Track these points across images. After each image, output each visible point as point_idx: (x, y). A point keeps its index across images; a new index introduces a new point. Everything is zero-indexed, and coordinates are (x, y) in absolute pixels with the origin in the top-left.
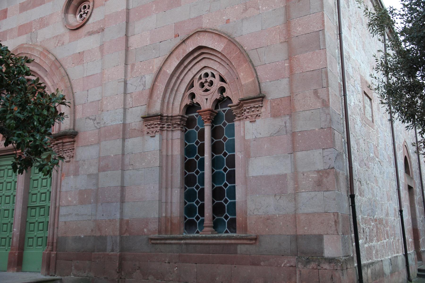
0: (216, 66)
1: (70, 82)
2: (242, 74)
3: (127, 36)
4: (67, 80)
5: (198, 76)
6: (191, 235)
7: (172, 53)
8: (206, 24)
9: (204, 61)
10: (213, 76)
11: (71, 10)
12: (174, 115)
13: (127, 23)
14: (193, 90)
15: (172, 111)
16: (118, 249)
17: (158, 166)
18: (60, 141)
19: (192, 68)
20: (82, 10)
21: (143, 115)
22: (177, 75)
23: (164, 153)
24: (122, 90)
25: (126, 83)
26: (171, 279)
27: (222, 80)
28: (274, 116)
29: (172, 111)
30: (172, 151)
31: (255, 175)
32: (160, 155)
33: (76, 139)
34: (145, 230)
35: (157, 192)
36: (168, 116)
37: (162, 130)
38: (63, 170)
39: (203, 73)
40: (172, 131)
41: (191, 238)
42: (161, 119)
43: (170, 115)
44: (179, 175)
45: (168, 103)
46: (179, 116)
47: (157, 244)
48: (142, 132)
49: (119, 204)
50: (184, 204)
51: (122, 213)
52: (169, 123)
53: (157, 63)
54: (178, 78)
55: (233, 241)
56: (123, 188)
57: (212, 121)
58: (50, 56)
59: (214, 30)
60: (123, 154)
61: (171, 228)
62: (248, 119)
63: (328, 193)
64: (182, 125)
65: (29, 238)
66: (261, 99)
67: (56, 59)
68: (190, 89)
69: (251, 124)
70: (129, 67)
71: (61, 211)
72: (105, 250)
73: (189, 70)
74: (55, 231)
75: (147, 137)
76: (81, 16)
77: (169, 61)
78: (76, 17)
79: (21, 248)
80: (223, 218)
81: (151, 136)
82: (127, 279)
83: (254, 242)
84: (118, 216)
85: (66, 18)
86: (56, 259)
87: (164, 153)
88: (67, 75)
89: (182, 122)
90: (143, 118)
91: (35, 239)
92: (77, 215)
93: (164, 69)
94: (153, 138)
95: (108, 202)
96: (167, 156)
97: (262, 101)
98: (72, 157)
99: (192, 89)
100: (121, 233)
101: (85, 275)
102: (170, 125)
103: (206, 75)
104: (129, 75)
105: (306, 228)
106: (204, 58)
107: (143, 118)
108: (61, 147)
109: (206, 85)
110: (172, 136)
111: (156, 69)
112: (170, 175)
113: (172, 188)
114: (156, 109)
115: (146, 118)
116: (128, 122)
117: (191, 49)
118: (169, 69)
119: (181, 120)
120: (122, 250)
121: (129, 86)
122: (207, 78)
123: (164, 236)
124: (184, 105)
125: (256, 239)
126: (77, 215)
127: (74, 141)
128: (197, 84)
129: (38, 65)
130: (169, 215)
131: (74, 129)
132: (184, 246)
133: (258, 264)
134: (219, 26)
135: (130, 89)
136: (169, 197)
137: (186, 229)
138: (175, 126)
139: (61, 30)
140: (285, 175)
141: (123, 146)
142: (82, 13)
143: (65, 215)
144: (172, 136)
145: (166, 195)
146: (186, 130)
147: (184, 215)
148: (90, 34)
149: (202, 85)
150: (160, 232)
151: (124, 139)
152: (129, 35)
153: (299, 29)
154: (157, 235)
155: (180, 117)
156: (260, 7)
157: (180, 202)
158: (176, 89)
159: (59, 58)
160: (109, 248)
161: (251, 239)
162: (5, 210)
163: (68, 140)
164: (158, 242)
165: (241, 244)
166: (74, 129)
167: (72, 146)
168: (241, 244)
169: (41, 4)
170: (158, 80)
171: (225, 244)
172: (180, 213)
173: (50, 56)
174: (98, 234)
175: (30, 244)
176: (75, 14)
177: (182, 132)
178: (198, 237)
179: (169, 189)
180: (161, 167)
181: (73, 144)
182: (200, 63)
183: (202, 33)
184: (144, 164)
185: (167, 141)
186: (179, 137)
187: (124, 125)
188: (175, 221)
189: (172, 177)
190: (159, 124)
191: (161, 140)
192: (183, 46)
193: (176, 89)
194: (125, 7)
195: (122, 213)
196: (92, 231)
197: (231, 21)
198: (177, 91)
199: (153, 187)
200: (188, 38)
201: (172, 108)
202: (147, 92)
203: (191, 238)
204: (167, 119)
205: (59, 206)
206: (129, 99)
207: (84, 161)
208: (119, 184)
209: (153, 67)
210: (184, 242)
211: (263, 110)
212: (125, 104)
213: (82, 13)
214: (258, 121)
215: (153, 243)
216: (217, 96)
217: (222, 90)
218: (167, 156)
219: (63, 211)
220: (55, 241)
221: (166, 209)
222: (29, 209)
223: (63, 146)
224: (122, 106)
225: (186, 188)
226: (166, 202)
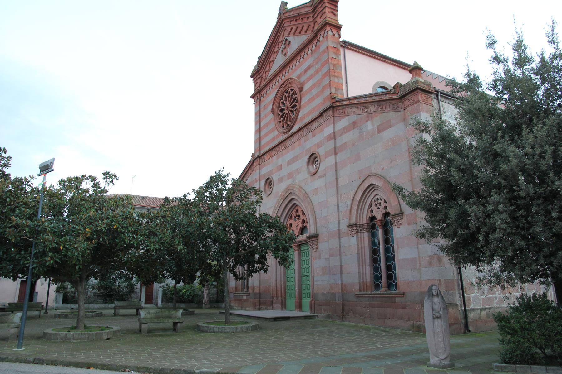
1: (313, 205)
2: (392, 200)
3: (336, 178)
4: (311, 205)
5: (374, 200)
6: (378, 292)
8: (373, 171)
10: (381, 200)
12: (363, 223)
13: (336, 171)
14: (372, 208)
16: (341, 300)
18: (311, 240)
19: (370, 195)
21: (347, 225)
22: (363, 200)
23: (360, 246)
24: (336, 210)
25: (338, 206)
26: (366, 316)
28: (409, 224)
31: (401, 258)
33: (318, 238)
34: (353, 289)
35: (357, 268)
36: (360, 225)
39: (376, 198)
40: (363, 232)
41: (374, 294)
43: (361, 224)
45: (360, 216)
48: (348, 234)
49: (340, 275)
50: (373, 274)
51: (342, 280)
54: (363, 202)
55: (393, 296)
56: (341, 266)
58: (303, 191)
59: (377, 174)
60: (340, 247)
61: (367, 288)
62: (396, 226)
63: (434, 268)
68: (370, 208)
69: (398, 229)
72: (335, 300)
75: (351, 237)
76: (316, 166)
79: (300, 299)
80: (392, 282)
82: (347, 316)
83: (403, 296)
86: (315, 305)
87: (360, 246)
88: (311, 201)
89: (368, 227)
90: (348, 226)
91: (306, 294)
93: (356, 197)
94: (353, 238)
95: (335, 274)
96: (362, 247)
97: (402, 215)
101: (328, 313)
103: (378, 199)
106: (375, 190)
107: (348, 226)
109: (378, 205)
110: (364, 235)
111: (352, 198)
112: (364, 258)
114: (354, 221)
115: (349, 226)
116: (341, 228)
117: (367, 186)
118: (358, 198)
120: (343, 301)
123: (362, 292)
124: (368, 217)
125: (404, 294)
126: (322, 281)
127: (317, 240)
128: (373, 204)
129: (296, 195)
132: (371, 298)
133: (405, 308)
134: (379, 172)
135: (341, 209)
137: (375, 288)
139: (307, 176)
140: (415, 258)
141: (340, 243)
142: (316, 164)
144: (364, 235)
146: (372, 231)
147: (373, 280)
148: (320, 177)
149: (376, 205)
150: (360, 291)
151: (340, 238)
154: (359, 292)
157: (370, 273)
159: (307, 191)
160: (337, 299)
161: (401, 294)
164: (359, 296)
166: (316, 233)
169: (296, 161)
171: (390, 297)
172: (371, 280)
173: (303, 191)
174: (332, 292)
175: (304, 296)
176: (313, 165)
179: (364, 266)
180: (358, 254)
183: (371, 176)
185: (361, 238)
186: (367, 236)
187: (339, 230)
188: (368, 284)
189: (365, 259)
190: (356, 229)
191: (357, 239)
193: (363, 208)
194: (334, 162)
195: (342, 280)
196: (329, 290)
197: (385, 169)
198: (364, 209)
200: (365, 179)
201: (362, 219)
203: (374, 294)
204: (360, 226)
206: (341, 216)
207: (323, 250)
211: (403, 220)
212: (339, 218)
213: (316, 164)
214: (401, 227)
215: (357, 297)
216: (384, 212)
217: (386, 208)
218: (362, 247)
219: (315, 279)
221: (363, 277)
223: (312, 242)
224: (337, 220)
226: (363, 274)
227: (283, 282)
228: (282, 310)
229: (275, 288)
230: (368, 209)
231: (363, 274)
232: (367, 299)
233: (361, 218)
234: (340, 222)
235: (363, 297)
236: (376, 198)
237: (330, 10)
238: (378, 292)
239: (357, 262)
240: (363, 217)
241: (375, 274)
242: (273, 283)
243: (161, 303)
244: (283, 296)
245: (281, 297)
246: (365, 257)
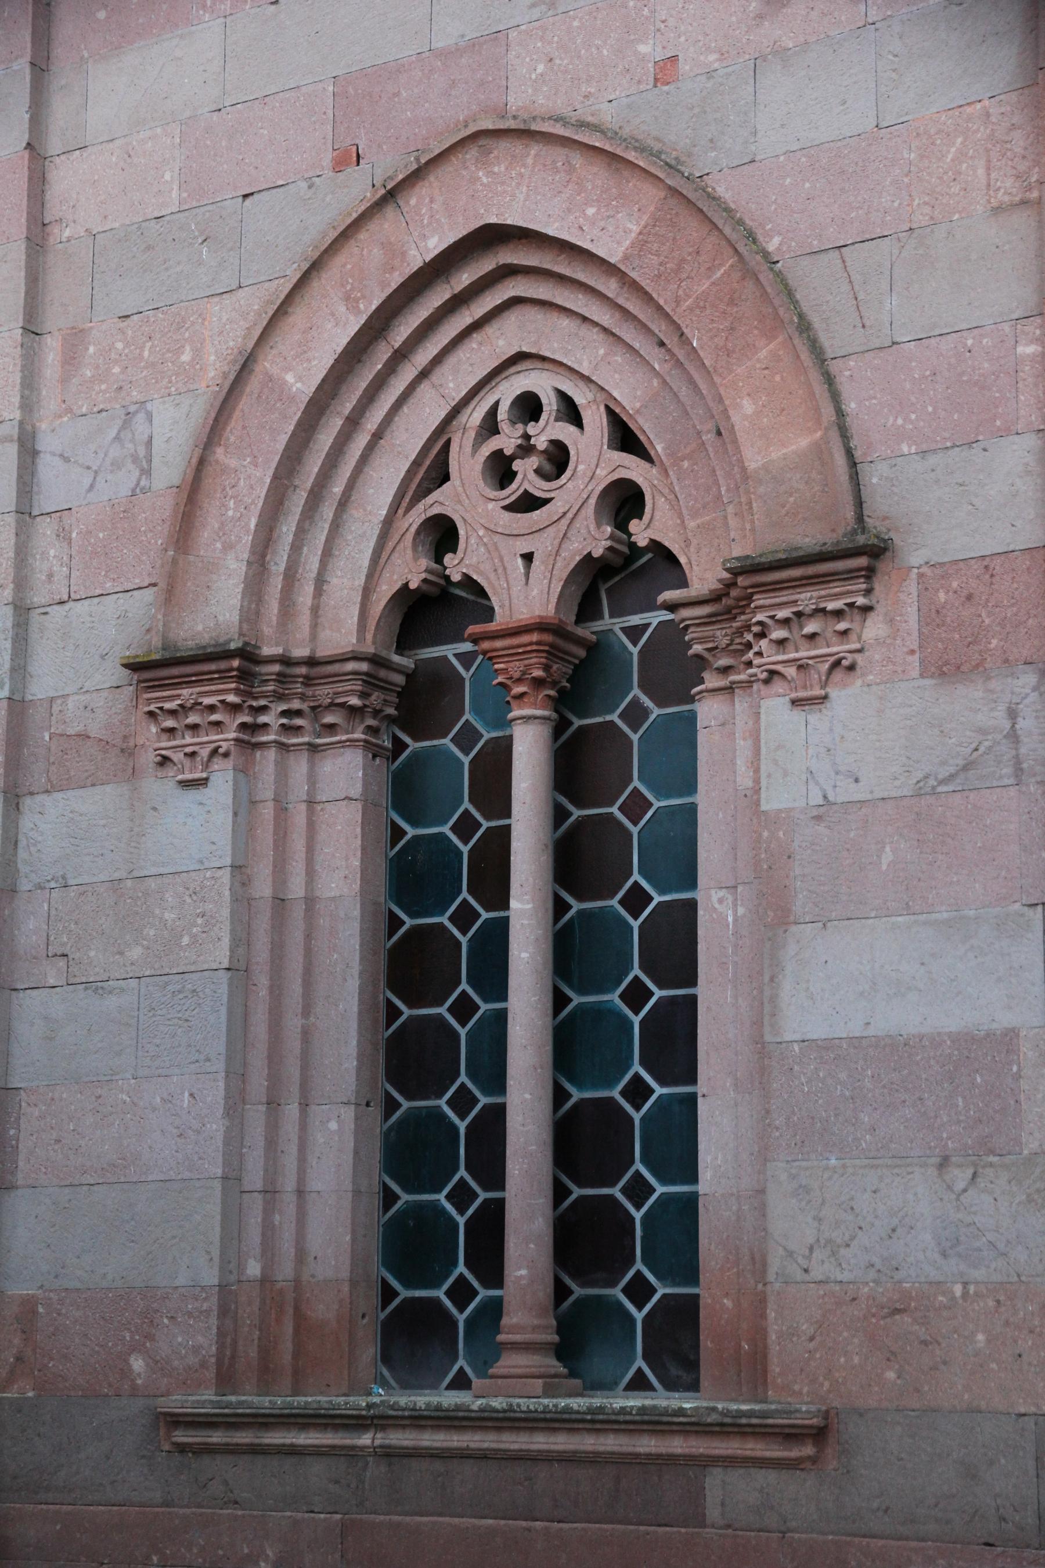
2: (748, 406)
5: (475, 415)
6: (422, 1400)
7: (315, 267)
9: (512, 319)
10: (571, 412)
12: (322, 653)
17: (226, 964)
19: (437, 360)
21: (137, 652)
23: (263, 888)
30: (310, 873)
31: (817, 1031)
34: (137, 1364)
35: (216, 1127)
36: (285, 661)
37: (248, 743)
39: (507, 391)
40: (313, 748)
41: (418, 1420)
42: (245, 676)
43: (300, 652)
44: (354, 1025)
45: (291, 576)
46: (356, 658)
48: (128, 752)
50: (376, 1202)
52: (296, 705)
54: (353, 422)
55: (677, 1445)
57: (562, 692)
62: (778, 686)
64: (376, 713)
66: (862, 561)
68: (423, 492)
69: (797, 716)
70: (52, 349)
77: (298, 317)
81: (180, 782)
83: (808, 1450)
87: (263, 888)
89: (376, 698)
90: (134, 667)
93: (268, 364)
94: (194, 795)
96: (280, 902)
97: (869, 573)
102: (299, 713)
107: (134, 667)
109: (525, 468)
110: (312, 779)
113: (304, 1105)
116: (39, 689)
117: (435, 245)
119: (371, 683)
121: (48, 468)
122: (532, 429)
124: (386, 590)
125: (819, 1434)
130: (285, 1271)
132: (375, 1470)
137: (386, 1358)
138: (329, 719)
144: (312, 779)
145: (272, 1144)
146: (399, 746)
152: (54, 145)
155: (364, 666)
157: (357, 1193)
158: (337, 489)
161: (791, 1435)
164: (217, 1437)
165: (730, 1462)
168: (730, 1462)
170: (232, 433)
177: (374, 756)
178: (461, 1414)
179: (292, 1110)
182: (490, 330)
183: (504, 145)
184: (136, 953)
185: (281, 810)
189: (306, 1035)
190: (234, 708)
192: (387, 224)
193: (337, 489)
197: (684, 67)
199: (191, 1095)
203: (418, 1420)
204: (282, 678)
209: (198, 353)
210: (377, 1442)
211: (873, 629)
212: (21, 582)
218: (280, 902)
221: (269, 1230)
225: (391, 1105)
226: (270, 1192)
230: (394, 509)
232: (317, 1470)
233: (305, 596)
234: (35, 616)
235: (255, 1450)
236: (507, 391)
238: (422, 1400)
239: (219, 1065)
240: (319, 592)
241: (405, 1197)
242: (316, 1240)
246: (307, 1010)
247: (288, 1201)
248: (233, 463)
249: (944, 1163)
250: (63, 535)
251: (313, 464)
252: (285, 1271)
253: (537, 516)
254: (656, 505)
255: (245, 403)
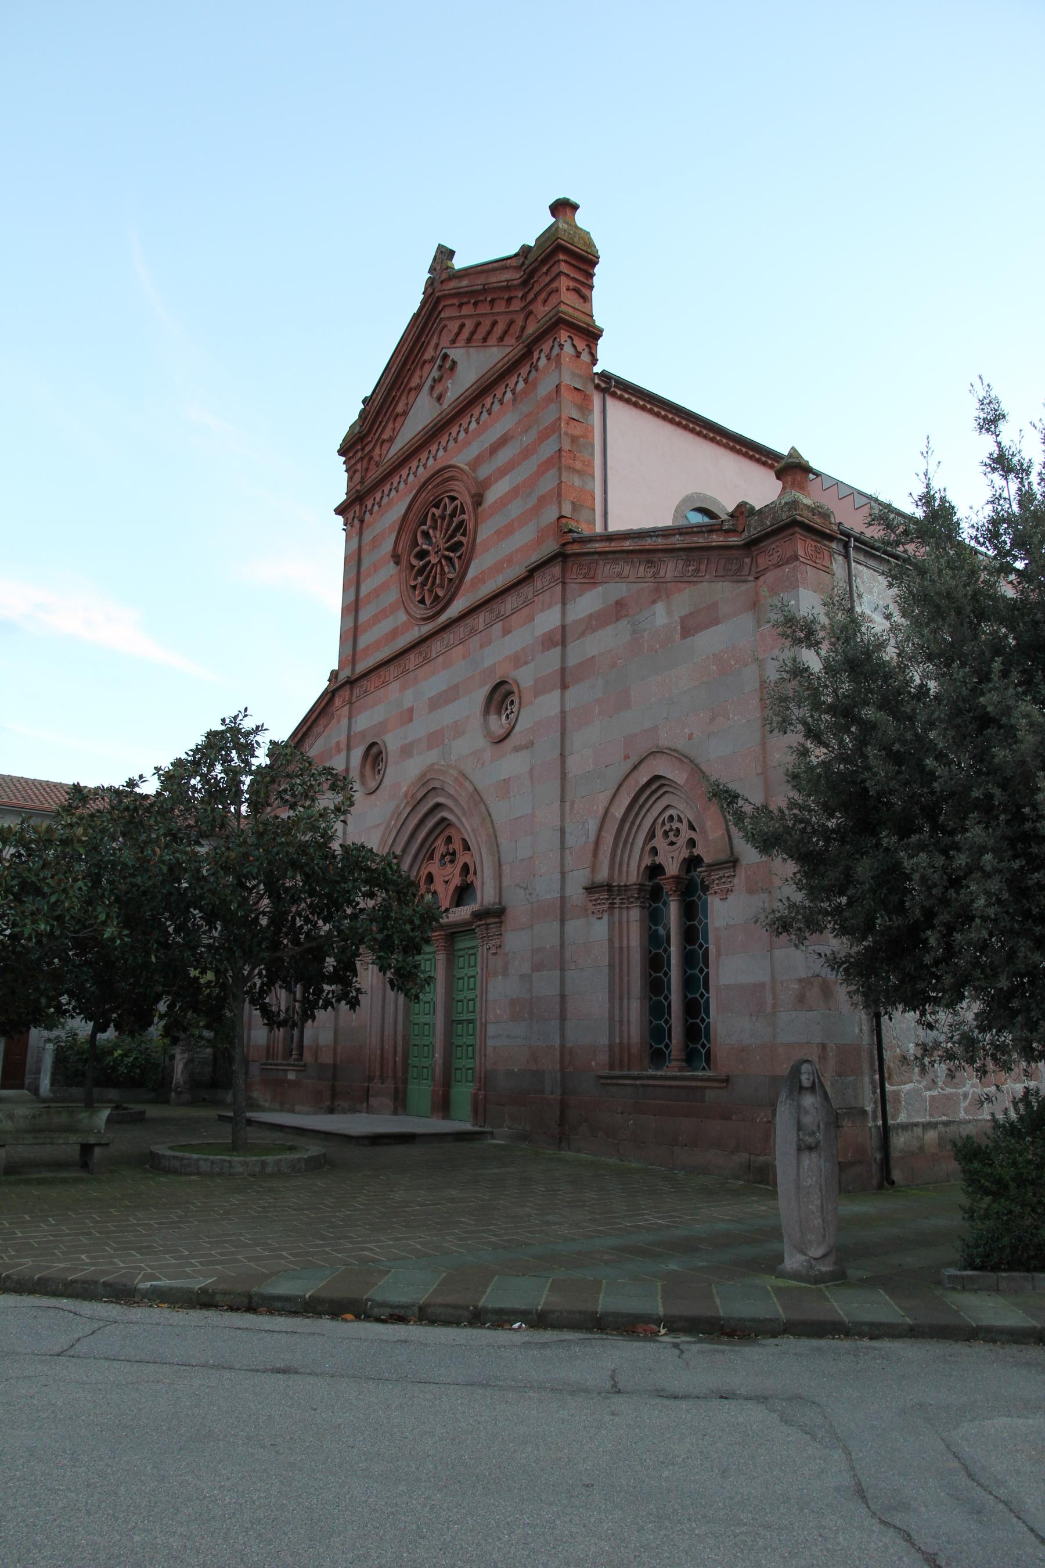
0: (682, 806)
3: (563, 756)
4: (489, 825)
5: (660, 820)
7: (620, 786)
8: (664, 739)
9: (666, 796)
10: (680, 820)
11: (493, 709)
12: (628, 884)
13: (563, 734)
14: (654, 843)
15: (627, 877)
18: (483, 922)
19: (651, 806)
20: (509, 707)
21: (584, 885)
27: (692, 827)
28: (751, 891)
29: (627, 877)
30: (628, 940)
32: (609, 948)
33: (503, 918)
34: (593, 1063)
35: (607, 1006)
36: (619, 886)
38: (489, 967)
40: (628, 908)
44: (639, 979)
45: (621, 864)
46: (636, 885)
47: (608, 1084)
48: (586, 910)
49: (558, 1022)
51: (563, 1036)
52: (623, 897)
53: (603, 799)
55: (699, 1084)
56: (563, 997)
57: (682, 892)
58: (467, 784)
60: (562, 945)
62: (717, 895)
63: (811, 1013)
64: (643, 898)
65: (457, 1069)
66: (731, 864)
67: (475, 789)
68: (650, 840)
70: (568, 805)
71: (489, 1030)
73: (648, 810)
74: (483, 1061)
77: (618, 798)
78: (501, 720)
83: (724, 1085)
84: (557, 1042)
85: (486, 722)
87: (617, 945)
88: (490, 815)
89: (642, 894)
90: (586, 889)
92: (508, 1036)
93: (612, 810)
96: (621, 948)
98: (500, 946)
99: (653, 841)
100: (562, 1068)
104: (568, 820)
105: (784, 1066)
107: (586, 889)
108: (484, 931)
109: (671, 834)
112: (625, 979)
113: (629, 999)
116: (568, 893)
117: (645, 780)
118: (618, 812)
119: (640, 891)
121: (568, 836)
122: (672, 824)
123: (617, 1073)
124: (642, 869)
126: (508, 1036)
127: (501, 922)
128: (659, 833)
130: (625, 1041)
131: (500, 903)
134: (680, 744)
135: (570, 841)
136: (625, 1013)
138: (631, 900)
140: (763, 985)
142: (508, 712)
143: (493, 1037)
146: (651, 905)
148: (517, 749)
149: (666, 834)
150: (612, 1067)
151: (562, 923)
152: (567, 753)
153: (777, 756)
154: (608, 1071)
156: (731, 716)
157: (641, 1021)
158: (630, 840)
161: (722, 1081)
162: (425, 1024)
163: (493, 920)
164: (609, 1081)
165: (710, 1088)
166: (500, 903)
167: (498, 929)
168: (710, 1088)
170: (605, 827)
173: (467, 784)
179: (625, 1001)
180: (611, 966)
181: (500, 926)
182: (662, 799)
183: (659, 754)
184: (589, 961)
187: (563, 898)
188: (634, 1050)
189: (629, 982)
190: (607, 899)
192: (635, 775)
193: (630, 840)
194: (558, 710)
195: (563, 1036)
200: (640, 762)
202: (590, 847)
205: (486, 1022)
206: (569, 859)
207: (514, 953)
208: (557, 992)
209: (597, 807)
211: (736, 881)
213: (508, 712)
215: (603, 1084)
216: (685, 854)
217: (692, 843)
218: (621, 948)
219: (491, 1030)
220: (483, 1075)
221: (621, 1031)
222: (455, 1024)
223: (487, 929)
224: (559, 870)
225: (651, 999)
226: (621, 1021)
227: (400, 1037)
228: (395, 1113)
229: (378, 1052)
231: (621, 1021)
234: (566, 875)
237: (572, 284)
238: (659, 1073)
243: (48, 1087)
244: (400, 1075)
245: (395, 1077)
247: (625, 1023)
248: (605, 835)
249: (751, 1015)
250: (571, 854)
251: (624, 835)
252: (625, 1041)
253: (674, 846)
254: (700, 844)
255: (608, 820)
